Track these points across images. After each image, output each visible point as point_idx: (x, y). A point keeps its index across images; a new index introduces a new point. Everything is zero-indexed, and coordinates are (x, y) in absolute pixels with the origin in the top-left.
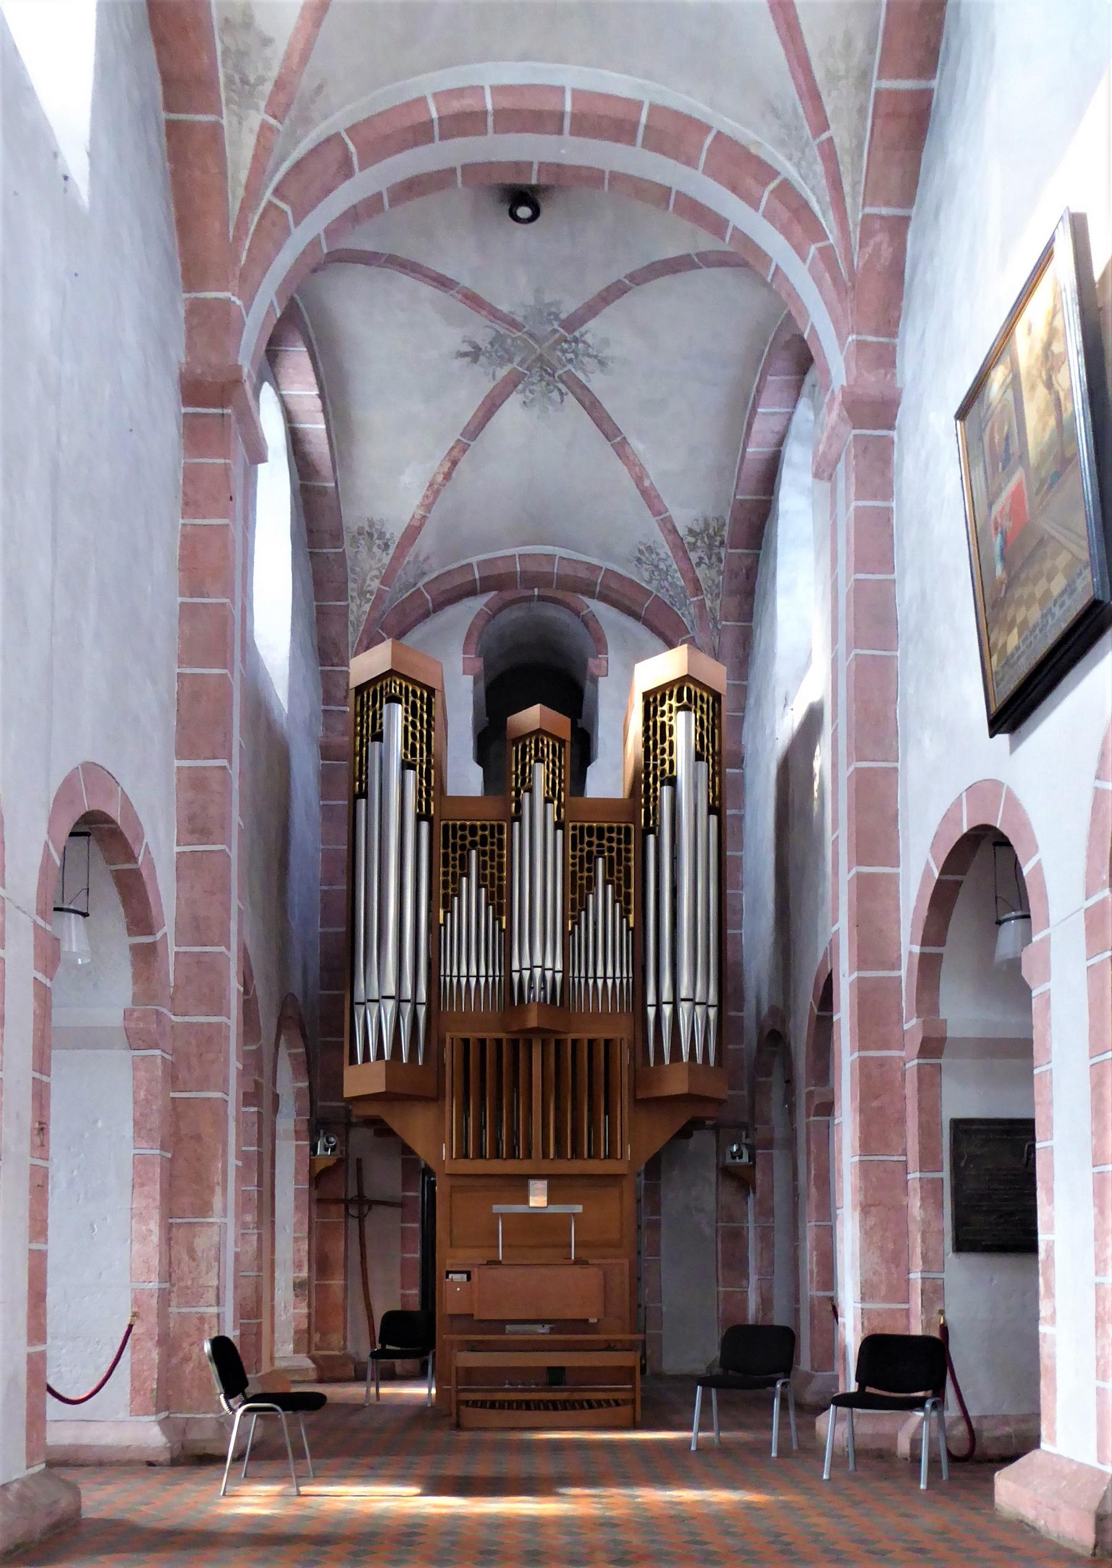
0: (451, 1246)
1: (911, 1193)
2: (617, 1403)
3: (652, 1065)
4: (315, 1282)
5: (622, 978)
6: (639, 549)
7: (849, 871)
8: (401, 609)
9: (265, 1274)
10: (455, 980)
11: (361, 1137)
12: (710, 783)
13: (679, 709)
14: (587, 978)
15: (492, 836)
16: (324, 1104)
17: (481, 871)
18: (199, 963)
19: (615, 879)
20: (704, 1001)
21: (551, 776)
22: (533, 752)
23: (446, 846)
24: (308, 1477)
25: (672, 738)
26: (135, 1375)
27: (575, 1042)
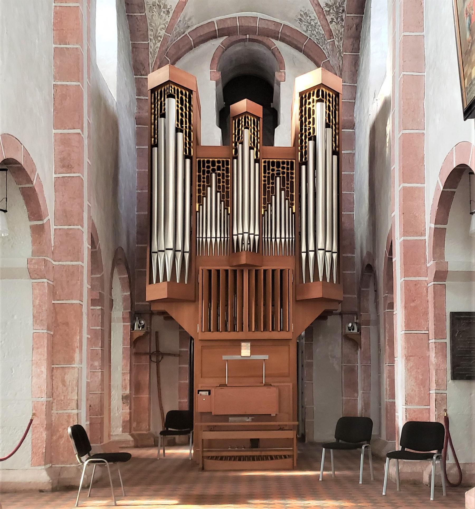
0: (201, 377)
1: (431, 350)
2: (285, 457)
3: (304, 283)
4: (134, 396)
5: (289, 238)
6: (301, 14)
7: (399, 186)
8: (177, 46)
9: (106, 392)
10: (204, 240)
11: (158, 320)
12: (334, 139)
13: (318, 101)
14: (271, 238)
15: (223, 166)
16: (138, 303)
17: (218, 184)
18: (67, 234)
19: (285, 187)
20: (330, 250)
21: (252, 136)
22: (243, 123)
23: (199, 171)
24: (122, 496)
25: (314, 116)
26: (34, 446)
27: (265, 271)
